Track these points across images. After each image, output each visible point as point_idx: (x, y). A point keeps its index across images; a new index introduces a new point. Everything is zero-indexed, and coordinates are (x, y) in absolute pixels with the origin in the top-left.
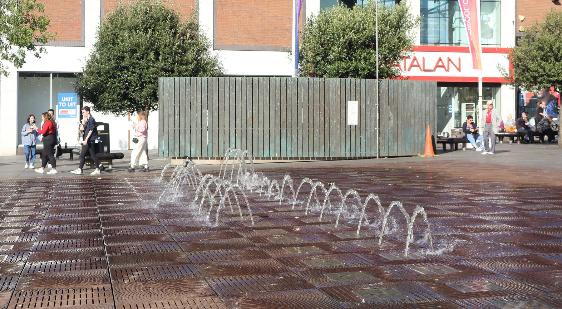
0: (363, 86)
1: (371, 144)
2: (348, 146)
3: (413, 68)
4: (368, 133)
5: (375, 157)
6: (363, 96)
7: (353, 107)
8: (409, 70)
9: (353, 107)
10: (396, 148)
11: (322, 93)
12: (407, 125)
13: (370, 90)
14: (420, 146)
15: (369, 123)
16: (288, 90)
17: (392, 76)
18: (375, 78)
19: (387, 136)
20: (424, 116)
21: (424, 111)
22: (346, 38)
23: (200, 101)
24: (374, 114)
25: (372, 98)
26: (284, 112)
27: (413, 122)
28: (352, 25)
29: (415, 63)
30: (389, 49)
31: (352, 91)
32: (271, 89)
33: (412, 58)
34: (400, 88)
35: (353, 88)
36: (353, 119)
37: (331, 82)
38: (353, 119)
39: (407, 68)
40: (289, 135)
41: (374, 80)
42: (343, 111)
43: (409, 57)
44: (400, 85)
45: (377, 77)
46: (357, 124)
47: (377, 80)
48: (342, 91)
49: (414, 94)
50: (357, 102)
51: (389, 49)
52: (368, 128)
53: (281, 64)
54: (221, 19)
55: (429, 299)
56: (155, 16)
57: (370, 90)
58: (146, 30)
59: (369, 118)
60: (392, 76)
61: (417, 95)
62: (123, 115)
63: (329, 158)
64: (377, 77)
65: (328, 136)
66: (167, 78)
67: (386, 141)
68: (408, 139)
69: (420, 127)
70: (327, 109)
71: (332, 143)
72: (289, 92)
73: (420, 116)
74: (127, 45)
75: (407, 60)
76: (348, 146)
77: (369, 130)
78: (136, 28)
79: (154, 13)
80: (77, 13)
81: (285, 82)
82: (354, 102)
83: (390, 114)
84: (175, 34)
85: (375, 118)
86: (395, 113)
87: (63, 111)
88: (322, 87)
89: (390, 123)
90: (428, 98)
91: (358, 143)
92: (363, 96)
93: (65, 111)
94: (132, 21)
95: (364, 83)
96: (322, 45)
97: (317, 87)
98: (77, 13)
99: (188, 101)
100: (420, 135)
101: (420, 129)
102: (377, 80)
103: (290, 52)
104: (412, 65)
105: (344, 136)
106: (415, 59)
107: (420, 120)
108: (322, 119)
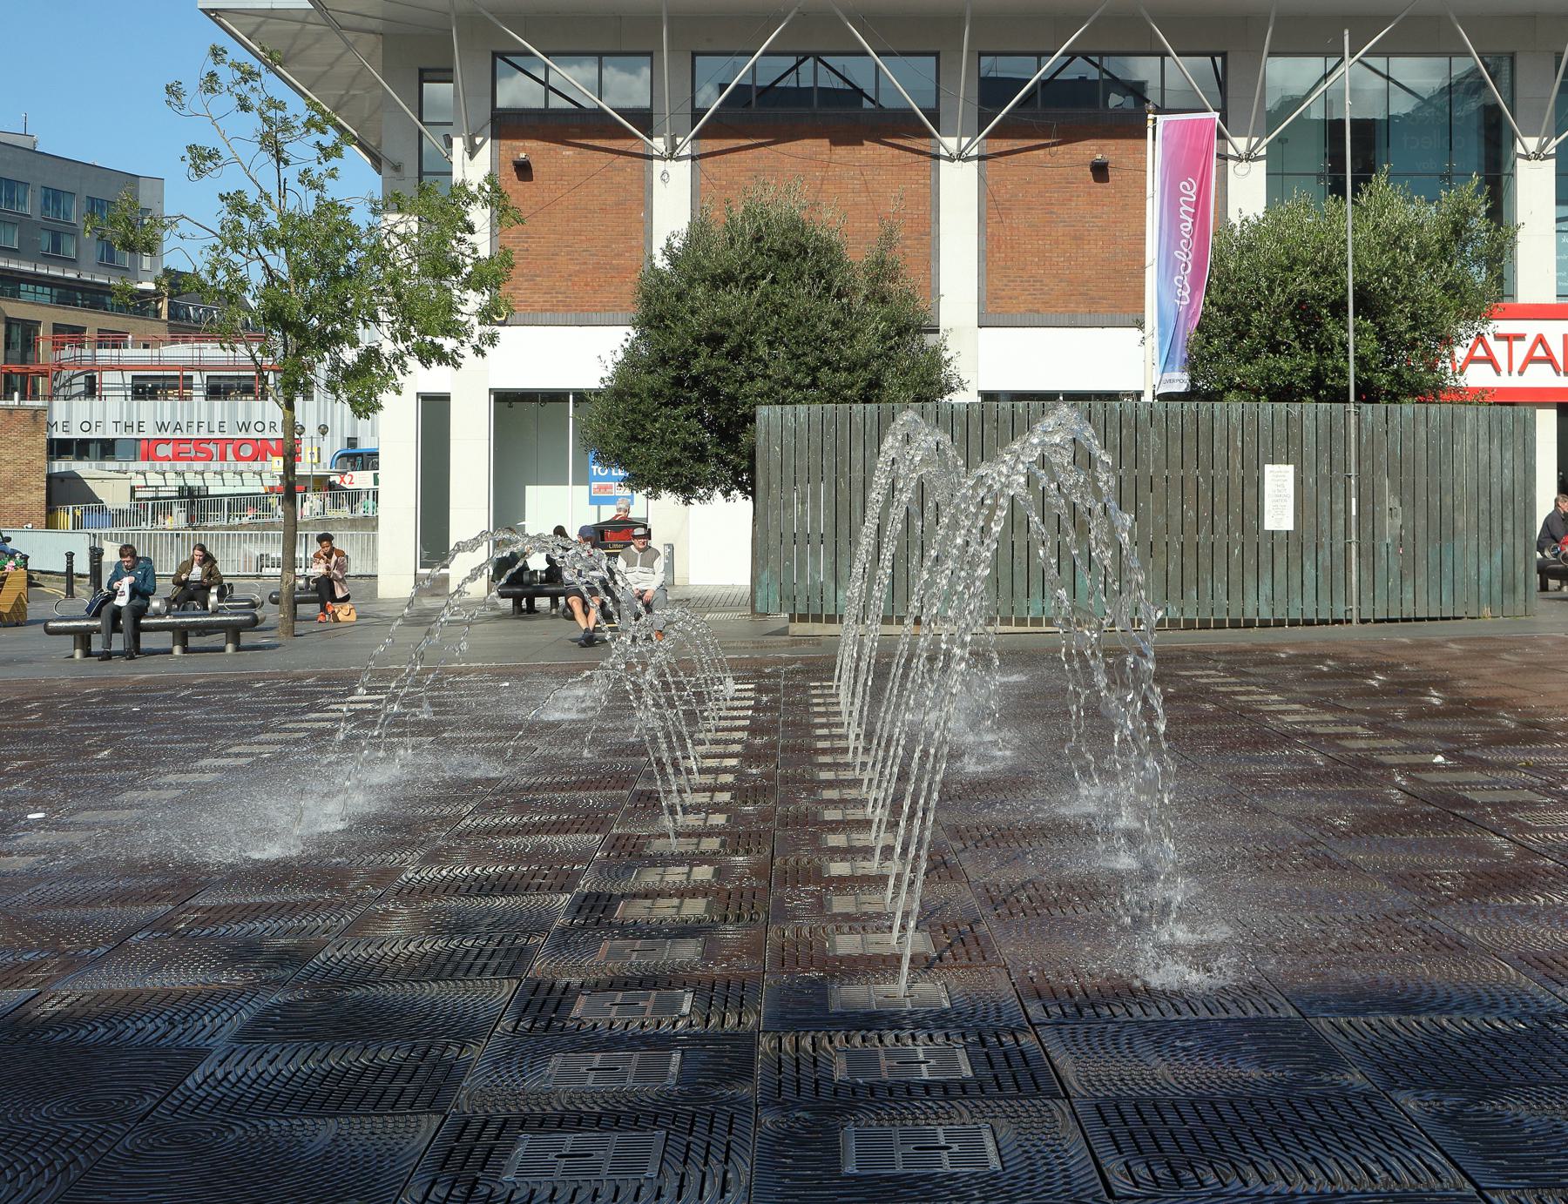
0: (1309, 423)
1: (1333, 580)
2: (1265, 589)
4: (1324, 555)
5: (1349, 621)
6: (1310, 450)
7: (1279, 482)
8: (1521, 373)
9: (1279, 482)
11: (1190, 445)
12: (1442, 530)
13: (1331, 435)
14: (1484, 589)
15: (1326, 526)
17: (1426, 390)
18: (1347, 400)
19: (1384, 562)
20: (1496, 506)
21: (1496, 490)
22: (1290, 288)
23: (859, 466)
24: (1342, 500)
25: (1338, 456)
27: (1460, 523)
29: (1540, 352)
30: (1414, 316)
31: (1277, 438)
33: (1530, 339)
35: (1281, 429)
36: (1279, 514)
37: (1217, 413)
38: (1279, 514)
41: (1341, 405)
42: (1250, 492)
43: (1521, 337)
44: (1423, 418)
45: (1352, 398)
46: (1291, 528)
47: (1352, 407)
48: (1247, 438)
49: (1464, 445)
50: (1291, 467)
51: (1414, 316)
52: (1325, 540)
53: (1127, 360)
54: (999, 248)
56: (777, 246)
57: (1331, 435)
58: (752, 282)
59: (1326, 513)
60: (1426, 390)
62: (700, 499)
63: (1190, 625)
64: (1352, 398)
65: (1208, 561)
66: (778, 407)
67: (1380, 574)
68: (1447, 570)
69: (1484, 535)
70: (1203, 486)
71: (1220, 581)
73: (1484, 505)
75: (1515, 343)
76: (1265, 589)
77: (1327, 546)
79: (775, 241)
80: (634, 243)
82: (1284, 467)
83: (1391, 501)
84: (828, 289)
85: (1347, 510)
86: (1407, 497)
87: (600, 488)
88: (1190, 429)
89: (1391, 526)
91: (1296, 582)
92: (1310, 450)
93: (606, 488)
94: (731, 258)
95: (1312, 416)
96: (1229, 310)
97: (1175, 427)
98: (634, 243)
101: (1483, 543)
102: (1352, 407)
103: (1140, 325)
104: (1531, 359)
105: (1253, 561)
106: (1540, 340)
107: (1484, 518)
108: (1191, 513)
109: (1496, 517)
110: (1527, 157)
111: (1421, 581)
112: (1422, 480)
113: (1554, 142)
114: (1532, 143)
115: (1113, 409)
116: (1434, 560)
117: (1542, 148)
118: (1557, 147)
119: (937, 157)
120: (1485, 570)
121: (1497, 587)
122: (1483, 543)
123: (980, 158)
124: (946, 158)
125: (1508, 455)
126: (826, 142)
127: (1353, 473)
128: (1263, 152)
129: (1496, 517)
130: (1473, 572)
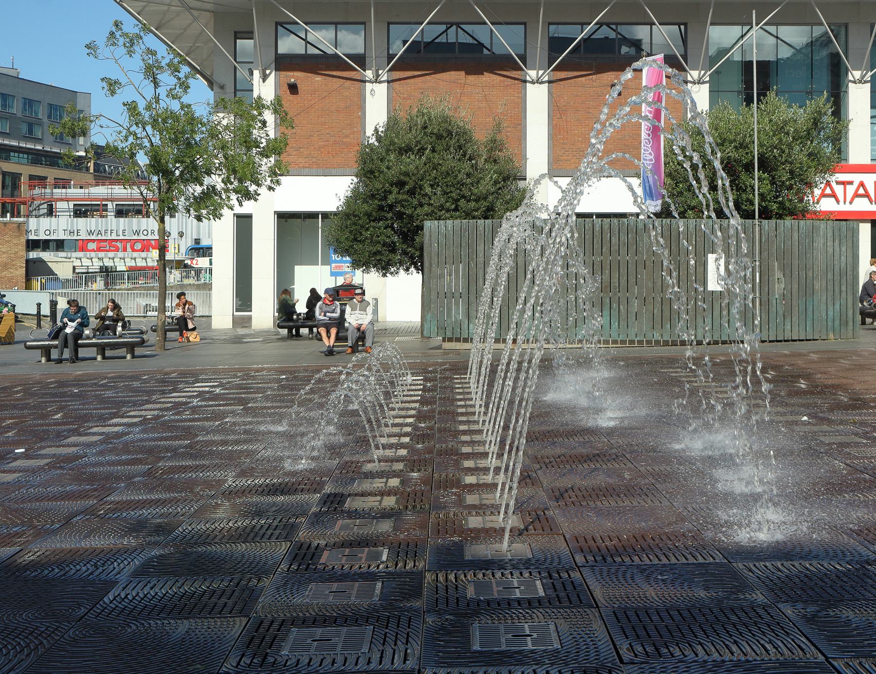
3: (856, 199)
8: (851, 203)
10: (789, 327)
12: (807, 290)
14: (830, 324)
16: (613, 238)
17: (799, 212)
18: (754, 218)
19: (774, 309)
20: (837, 278)
23: (482, 255)
26: (607, 272)
27: (817, 286)
28: (732, 137)
29: (861, 191)
32: (587, 237)
33: (856, 185)
34: (796, 235)
38: (714, 285)
39: (848, 199)
40: (615, 306)
41: (751, 221)
43: (851, 183)
44: (796, 228)
45: (757, 217)
47: (757, 222)
49: (819, 243)
55: (766, 567)
56: (435, 131)
61: (825, 244)
62: (392, 273)
64: (757, 217)
68: (810, 313)
69: (830, 293)
72: (615, 240)
73: (830, 276)
74: (392, 174)
75: (848, 186)
78: (408, 149)
79: (434, 128)
80: (355, 129)
81: (608, 225)
86: (788, 272)
87: (336, 267)
90: (844, 249)
98: (355, 129)
99: (465, 256)
100: (830, 307)
104: (856, 195)
106: (862, 184)
109: (837, 283)
110: (855, 82)
111: (795, 319)
112: (796, 263)
113: (870, 74)
114: (857, 74)
115: (624, 223)
116: (802, 307)
117: (863, 77)
118: (871, 76)
119: (525, 81)
120: (830, 313)
121: (837, 322)
122: (830, 298)
123: (549, 82)
124: (691, 82)
125: (844, 249)
126: (463, 73)
127: (757, 259)
128: (708, 79)
129: (837, 283)
130: (824, 315)
